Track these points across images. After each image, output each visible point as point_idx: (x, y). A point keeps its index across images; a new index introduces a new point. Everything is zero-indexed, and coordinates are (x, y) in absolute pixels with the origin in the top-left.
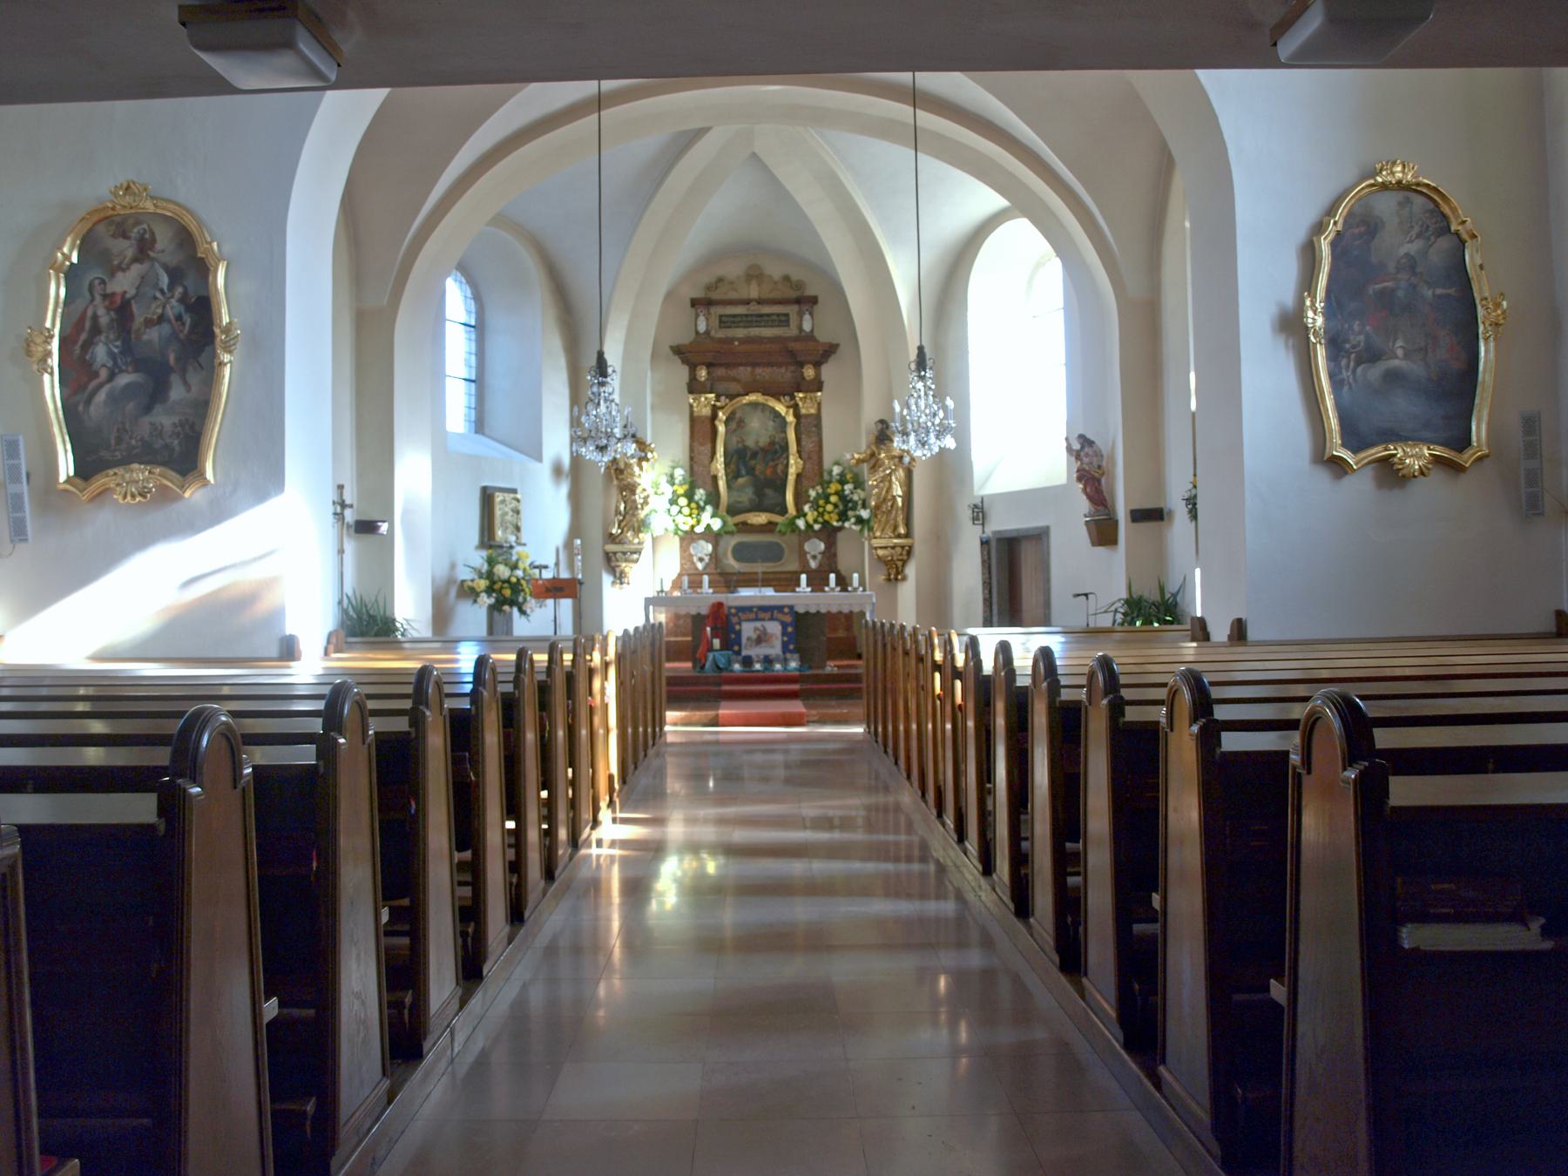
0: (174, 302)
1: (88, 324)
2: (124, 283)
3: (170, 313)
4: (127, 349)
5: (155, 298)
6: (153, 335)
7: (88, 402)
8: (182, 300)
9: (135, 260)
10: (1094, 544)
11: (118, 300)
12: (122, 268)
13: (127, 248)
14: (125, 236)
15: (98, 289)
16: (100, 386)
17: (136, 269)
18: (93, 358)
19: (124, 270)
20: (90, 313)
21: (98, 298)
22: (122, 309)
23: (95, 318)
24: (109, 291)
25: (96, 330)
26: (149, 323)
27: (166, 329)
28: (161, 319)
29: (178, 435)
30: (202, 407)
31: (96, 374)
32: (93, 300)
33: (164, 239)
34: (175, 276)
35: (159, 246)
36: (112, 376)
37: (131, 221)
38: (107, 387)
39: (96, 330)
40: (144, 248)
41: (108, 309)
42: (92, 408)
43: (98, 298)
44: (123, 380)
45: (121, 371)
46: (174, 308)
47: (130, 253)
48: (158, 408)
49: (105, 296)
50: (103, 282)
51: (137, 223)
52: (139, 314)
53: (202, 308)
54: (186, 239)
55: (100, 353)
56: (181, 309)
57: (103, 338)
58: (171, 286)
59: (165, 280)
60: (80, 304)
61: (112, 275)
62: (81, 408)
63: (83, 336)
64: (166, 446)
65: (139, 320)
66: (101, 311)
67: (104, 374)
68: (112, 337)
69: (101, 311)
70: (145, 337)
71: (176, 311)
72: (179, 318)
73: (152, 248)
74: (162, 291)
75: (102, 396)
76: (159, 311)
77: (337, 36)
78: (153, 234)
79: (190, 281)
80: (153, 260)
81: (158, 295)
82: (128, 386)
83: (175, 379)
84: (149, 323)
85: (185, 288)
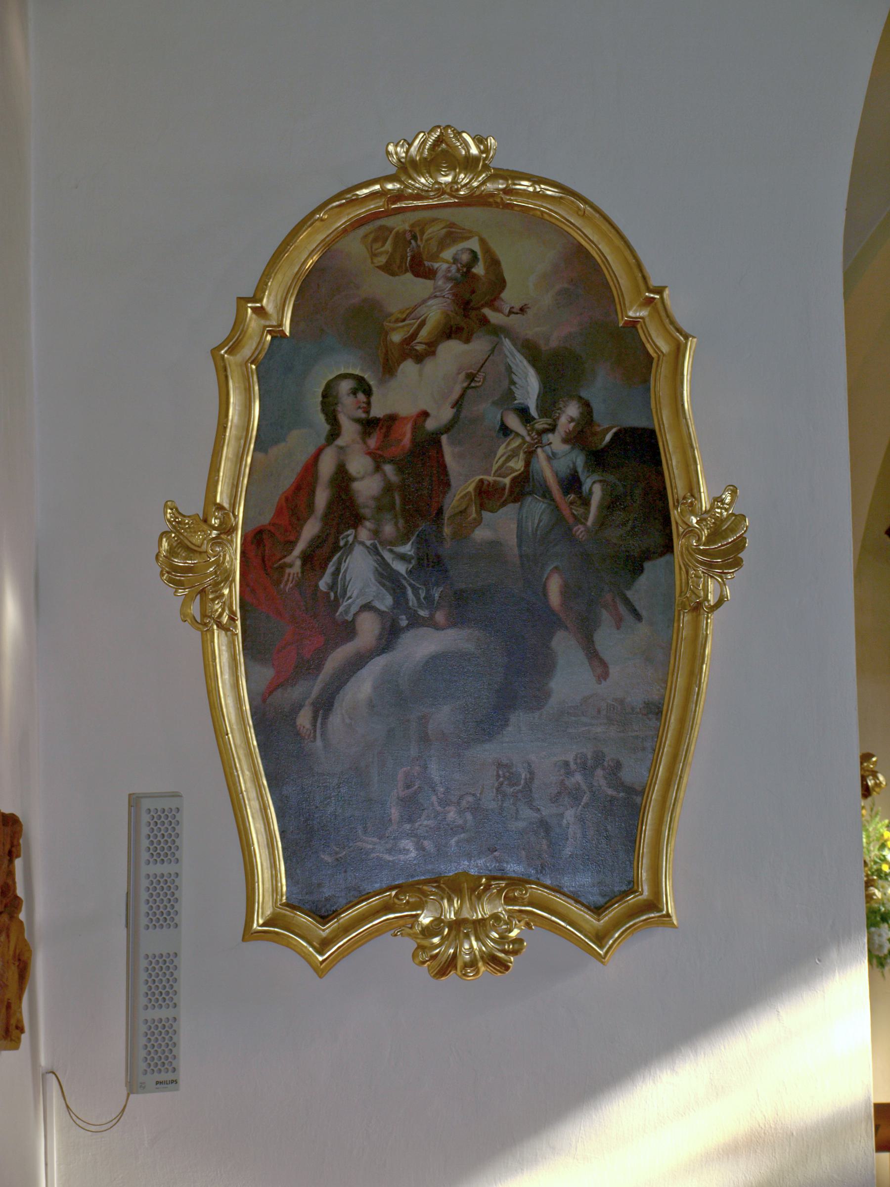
0: (555, 440)
1: (322, 497)
2: (417, 392)
3: (547, 470)
4: (430, 563)
5: (505, 431)
6: (501, 526)
7: (324, 706)
8: (579, 438)
9: (450, 332)
10: (16, 1048)
11: (406, 437)
12: (419, 353)
13: (426, 301)
14: (420, 268)
15: (349, 407)
16: (359, 662)
17: (452, 353)
18: (339, 589)
19: (419, 358)
20: (327, 467)
21: (349, 430)
22: (419, 461)
23: (342, 480)
24: (377, 411)
25: (345, 511)
26: (487, 495)
27: (536, 510)
28: (523, 486)
29: (575, 795)
30: (653, 718)
31: (349, 630)
32: (334, 433)
33: (527, 276)
34: (560, 372)
35: (510, 297)
36: (391, 635)
37: (435, 231)
38: (378, 664)
39: (345, 511)
40: (473, 303)
41: (378, 460)
42: (336, 720)
43: (349, 430)
44: (420, 646)
45: (415, 622)
46: (557, 457)
47: (435, 313)
48: (519, 719)
49: (369, 425)
50: (363, 387)
51: (453, 235)
52: (463, 474)
53: (635, 458)
54: (583, 275)
55: (358, 570)
56: (580, 460)
57: (364, 534)
58: (550, 402)
59: (530, 387)
60: (300, 444)
61: (389, 369)
62: (304, 720)
63: (311, 529)
64: (544, 826)
65: (463, 482)
66: (358, 464)
67: (368, 629)
68: (388, 529)
69: (358, 464)
70: (481, 534)
71: (563, 466)
72: (572, 484)
73: (493, 303)
74: (523, 413)
75: (363, 687)
76: (518, 465)
77: (571, 466)
78: (494, 263)
79: (602, 389)
80: (497, 331)
81: (513, 422)
82: (434, 662)
83: (565, 645)
84: (487, 495)
85: (586, 406)
